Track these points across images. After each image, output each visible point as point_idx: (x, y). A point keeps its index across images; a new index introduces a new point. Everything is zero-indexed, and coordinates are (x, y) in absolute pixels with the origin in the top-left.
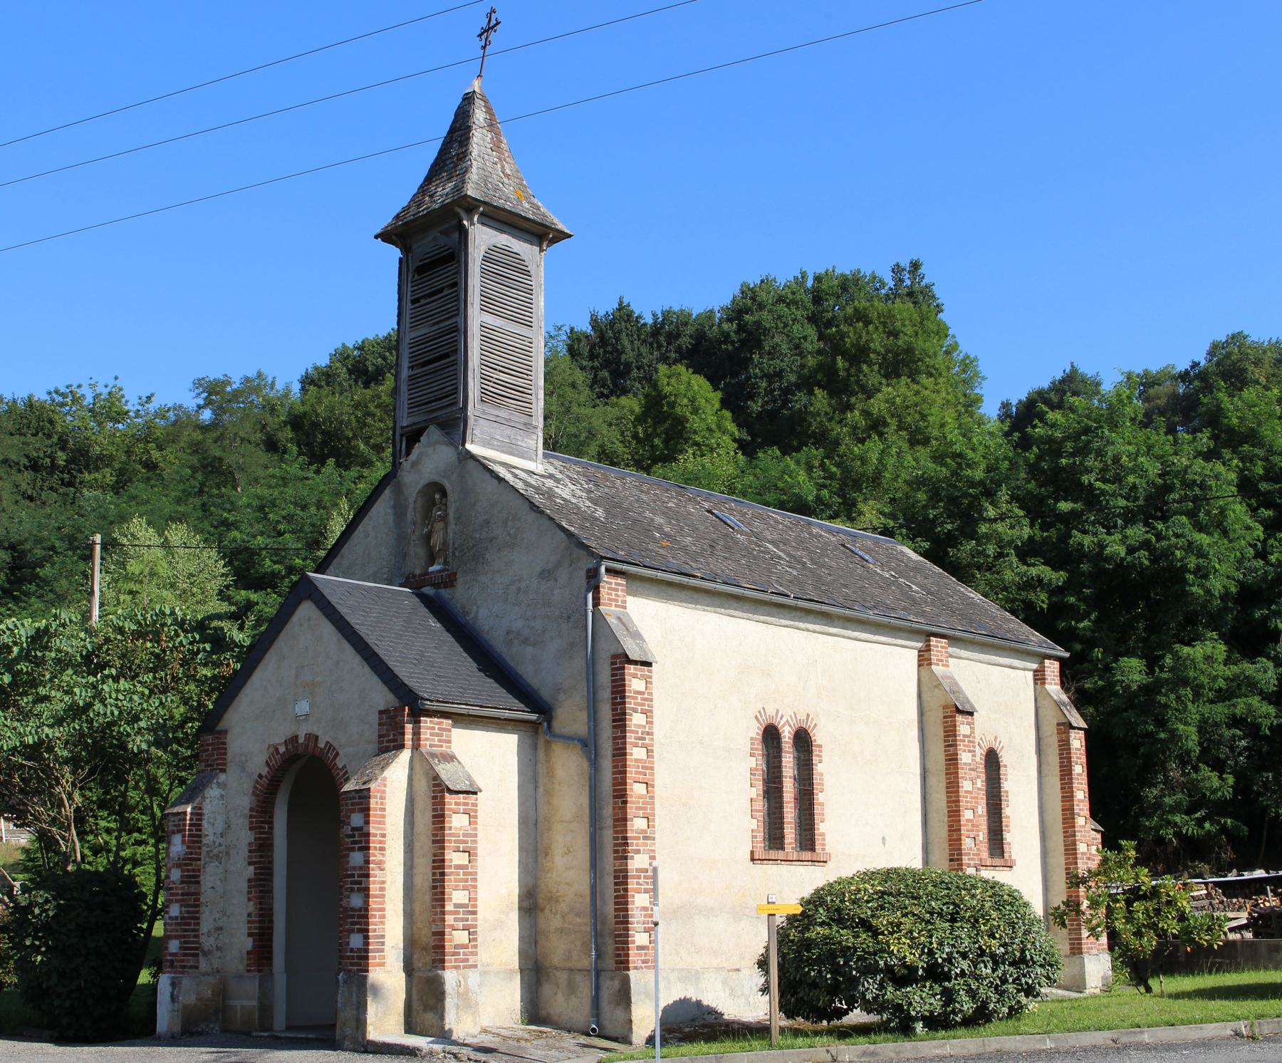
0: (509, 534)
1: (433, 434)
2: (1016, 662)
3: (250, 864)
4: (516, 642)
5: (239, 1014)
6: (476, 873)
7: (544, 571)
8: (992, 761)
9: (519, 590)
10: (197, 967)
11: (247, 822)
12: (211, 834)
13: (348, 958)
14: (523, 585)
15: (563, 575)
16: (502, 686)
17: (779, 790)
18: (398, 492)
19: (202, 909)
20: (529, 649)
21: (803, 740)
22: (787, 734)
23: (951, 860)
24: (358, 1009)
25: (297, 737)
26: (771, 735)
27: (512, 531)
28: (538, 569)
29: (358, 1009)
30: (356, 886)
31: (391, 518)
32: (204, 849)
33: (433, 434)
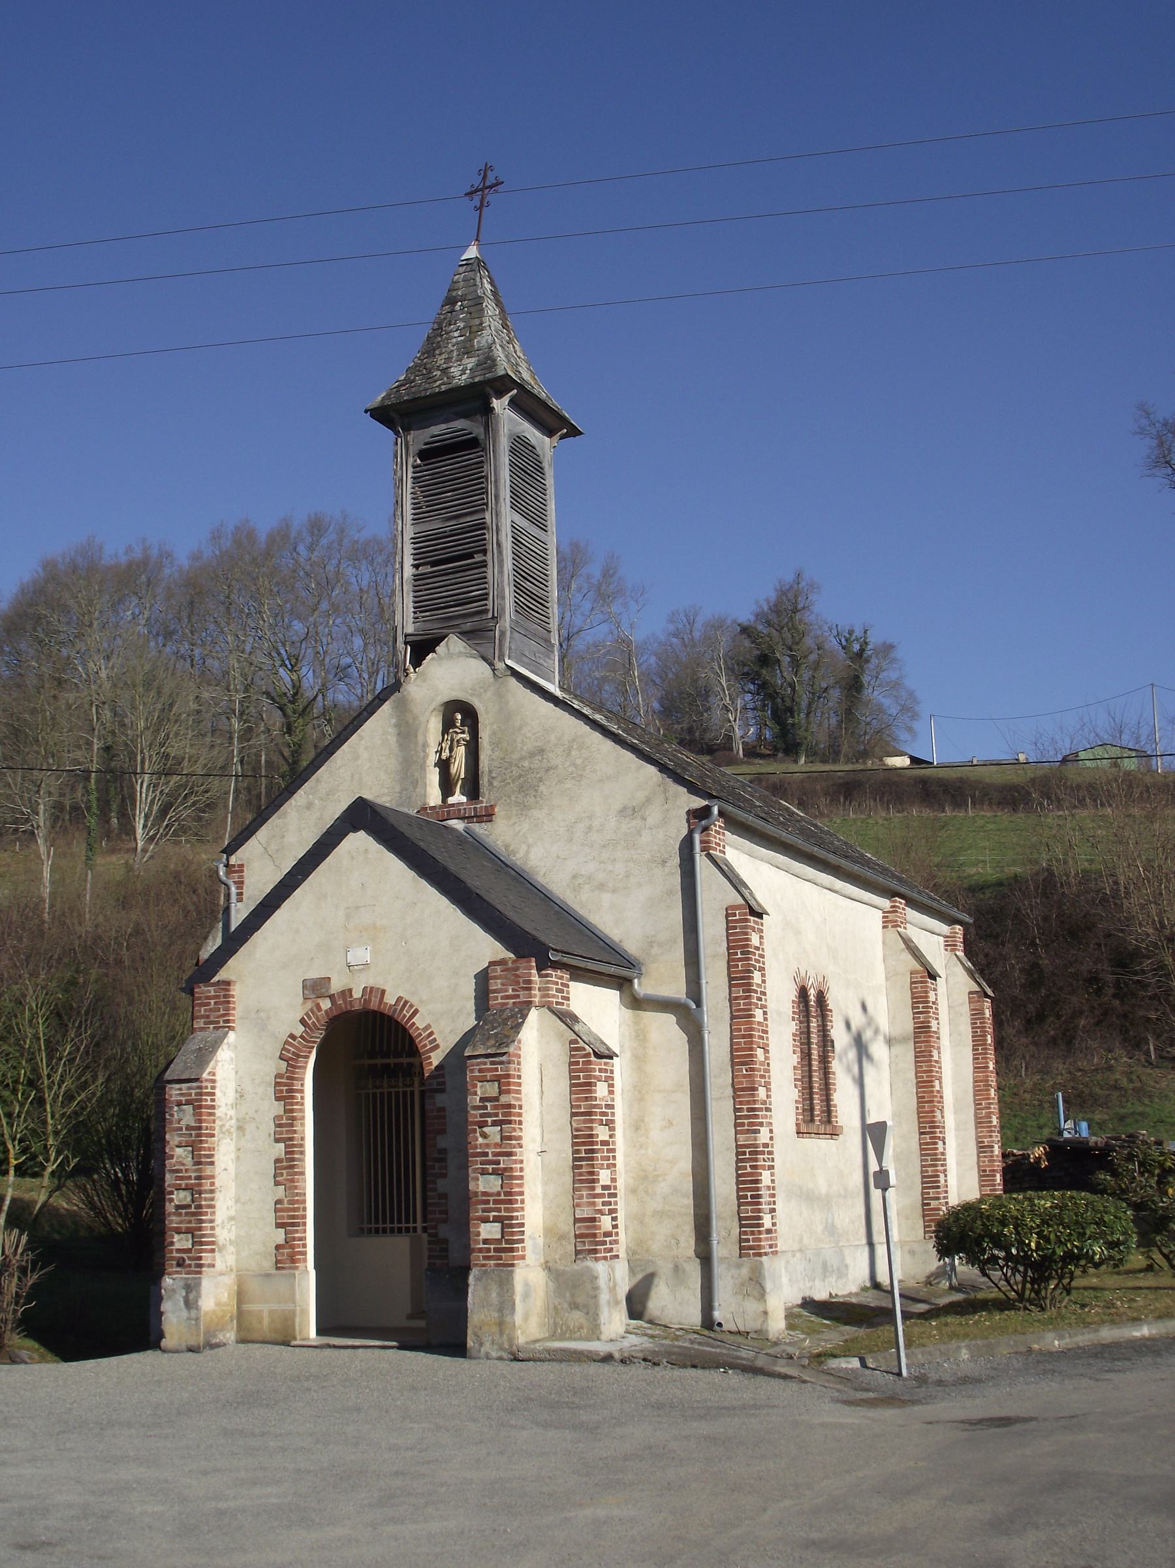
0: (575, 765)
1: (454, 643)
2: (839, 884)
3: (277, 1141)
4: (586, 887)
5: (266, 1322)
6: (945, 1160)
7: (624, 809)
8: (812, 1006)
9: (590, 828)
10: (213, 1266)
11: (271, 1091)
12: (223, 1105)
13: (480, 1250)
14: (596, 823)
15: (654, 815)
16: (278, 907)
17: (809, 1055)
18: (403, 708)
19: (217, 1195)
20: (606, 898)
21: (821, 997)
22: (812, 993)
23: (921, 1133)
24: (500, 1310)
25: (350, 990)
26: (803, 993)
27: (579, 762)
28: (618, 806)
29: (500, 1310)
30: (490, 1167)
31: (393, 739)
32: (218, 1123)
33: (454, 643)
